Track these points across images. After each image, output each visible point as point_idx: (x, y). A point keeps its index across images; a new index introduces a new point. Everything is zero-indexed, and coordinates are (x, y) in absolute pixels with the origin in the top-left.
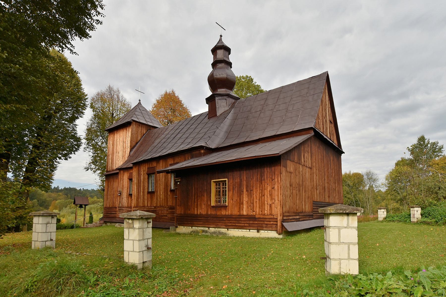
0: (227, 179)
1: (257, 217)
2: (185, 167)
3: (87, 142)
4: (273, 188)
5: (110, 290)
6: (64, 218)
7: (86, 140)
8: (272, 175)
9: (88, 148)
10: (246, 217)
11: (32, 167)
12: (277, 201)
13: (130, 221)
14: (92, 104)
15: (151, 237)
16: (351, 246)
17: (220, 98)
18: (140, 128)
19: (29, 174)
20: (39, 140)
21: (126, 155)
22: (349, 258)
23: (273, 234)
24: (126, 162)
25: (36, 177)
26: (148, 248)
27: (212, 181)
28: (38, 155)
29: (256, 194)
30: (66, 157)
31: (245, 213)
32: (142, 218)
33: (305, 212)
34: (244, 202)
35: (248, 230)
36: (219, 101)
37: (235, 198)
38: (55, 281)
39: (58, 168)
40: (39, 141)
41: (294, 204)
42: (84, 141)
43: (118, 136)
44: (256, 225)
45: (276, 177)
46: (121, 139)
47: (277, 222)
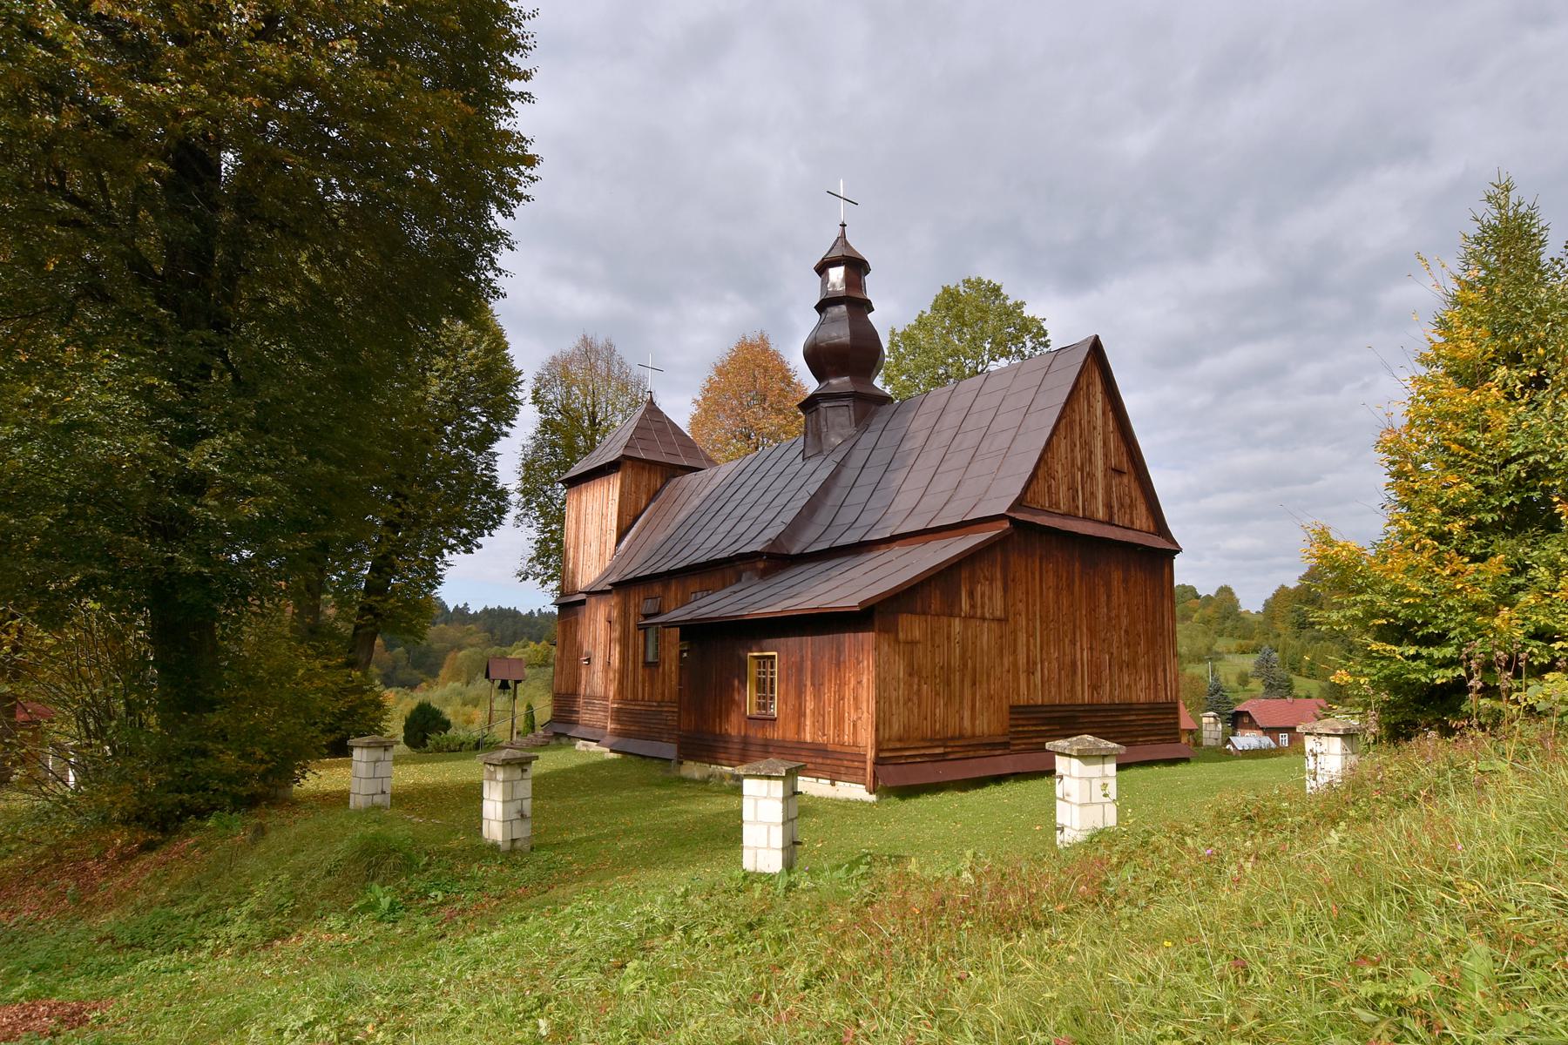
0: (775, 653)
1: (830, 748)
2: (691, 620)
3: (523, 500)
4: (860, 682)
5: (443, 878)
6: (476, 706)
7: (521, 496)
8: (858, 652)
9: (526, 515)
10: (810, 747)
11: (381, 581)
12: (865, 714)
13: (492, 768)
14: (536, 392)
15: (530, 795)
16: (772, 828)
17: (837, 404)
18: (646, 475)
19: (373, 598)
20: (399, 506)
21: (608, 551)
22: (768, 847)
23: (856, 792)
24: (606, 573)
25: (390, 607)
26: (523, 816)
27: (750, 654)
28: (396, 545)
29: (829, 695)
30: (468, 545)
31: (808, 738)
32: (508, 764)
34: (808, 711)
35: (814, 780)
36: (830, 414)
37: (792, 700)
38: (366, 860)
39: (445, 579)
40: (398, 510)
41: (926, 719)
42: (515, 497)
43: (590, 498)
44: (827, 768)
45: (866, 656)
46: (596, 506)
47: (865, 762)
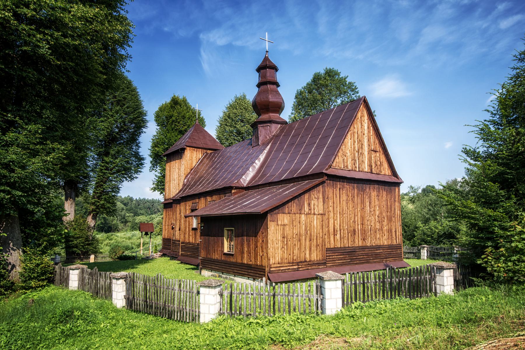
0: (233, 228)
18: (195, 153)
33: (310, 261)
34: (245, 251)
47: (265, 272)
